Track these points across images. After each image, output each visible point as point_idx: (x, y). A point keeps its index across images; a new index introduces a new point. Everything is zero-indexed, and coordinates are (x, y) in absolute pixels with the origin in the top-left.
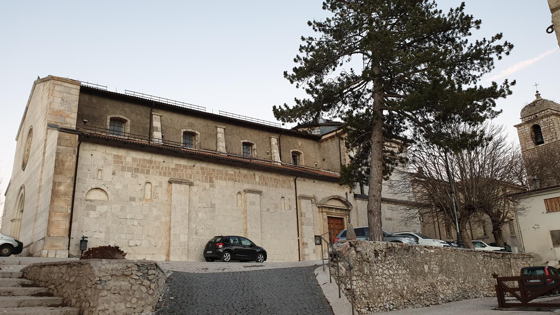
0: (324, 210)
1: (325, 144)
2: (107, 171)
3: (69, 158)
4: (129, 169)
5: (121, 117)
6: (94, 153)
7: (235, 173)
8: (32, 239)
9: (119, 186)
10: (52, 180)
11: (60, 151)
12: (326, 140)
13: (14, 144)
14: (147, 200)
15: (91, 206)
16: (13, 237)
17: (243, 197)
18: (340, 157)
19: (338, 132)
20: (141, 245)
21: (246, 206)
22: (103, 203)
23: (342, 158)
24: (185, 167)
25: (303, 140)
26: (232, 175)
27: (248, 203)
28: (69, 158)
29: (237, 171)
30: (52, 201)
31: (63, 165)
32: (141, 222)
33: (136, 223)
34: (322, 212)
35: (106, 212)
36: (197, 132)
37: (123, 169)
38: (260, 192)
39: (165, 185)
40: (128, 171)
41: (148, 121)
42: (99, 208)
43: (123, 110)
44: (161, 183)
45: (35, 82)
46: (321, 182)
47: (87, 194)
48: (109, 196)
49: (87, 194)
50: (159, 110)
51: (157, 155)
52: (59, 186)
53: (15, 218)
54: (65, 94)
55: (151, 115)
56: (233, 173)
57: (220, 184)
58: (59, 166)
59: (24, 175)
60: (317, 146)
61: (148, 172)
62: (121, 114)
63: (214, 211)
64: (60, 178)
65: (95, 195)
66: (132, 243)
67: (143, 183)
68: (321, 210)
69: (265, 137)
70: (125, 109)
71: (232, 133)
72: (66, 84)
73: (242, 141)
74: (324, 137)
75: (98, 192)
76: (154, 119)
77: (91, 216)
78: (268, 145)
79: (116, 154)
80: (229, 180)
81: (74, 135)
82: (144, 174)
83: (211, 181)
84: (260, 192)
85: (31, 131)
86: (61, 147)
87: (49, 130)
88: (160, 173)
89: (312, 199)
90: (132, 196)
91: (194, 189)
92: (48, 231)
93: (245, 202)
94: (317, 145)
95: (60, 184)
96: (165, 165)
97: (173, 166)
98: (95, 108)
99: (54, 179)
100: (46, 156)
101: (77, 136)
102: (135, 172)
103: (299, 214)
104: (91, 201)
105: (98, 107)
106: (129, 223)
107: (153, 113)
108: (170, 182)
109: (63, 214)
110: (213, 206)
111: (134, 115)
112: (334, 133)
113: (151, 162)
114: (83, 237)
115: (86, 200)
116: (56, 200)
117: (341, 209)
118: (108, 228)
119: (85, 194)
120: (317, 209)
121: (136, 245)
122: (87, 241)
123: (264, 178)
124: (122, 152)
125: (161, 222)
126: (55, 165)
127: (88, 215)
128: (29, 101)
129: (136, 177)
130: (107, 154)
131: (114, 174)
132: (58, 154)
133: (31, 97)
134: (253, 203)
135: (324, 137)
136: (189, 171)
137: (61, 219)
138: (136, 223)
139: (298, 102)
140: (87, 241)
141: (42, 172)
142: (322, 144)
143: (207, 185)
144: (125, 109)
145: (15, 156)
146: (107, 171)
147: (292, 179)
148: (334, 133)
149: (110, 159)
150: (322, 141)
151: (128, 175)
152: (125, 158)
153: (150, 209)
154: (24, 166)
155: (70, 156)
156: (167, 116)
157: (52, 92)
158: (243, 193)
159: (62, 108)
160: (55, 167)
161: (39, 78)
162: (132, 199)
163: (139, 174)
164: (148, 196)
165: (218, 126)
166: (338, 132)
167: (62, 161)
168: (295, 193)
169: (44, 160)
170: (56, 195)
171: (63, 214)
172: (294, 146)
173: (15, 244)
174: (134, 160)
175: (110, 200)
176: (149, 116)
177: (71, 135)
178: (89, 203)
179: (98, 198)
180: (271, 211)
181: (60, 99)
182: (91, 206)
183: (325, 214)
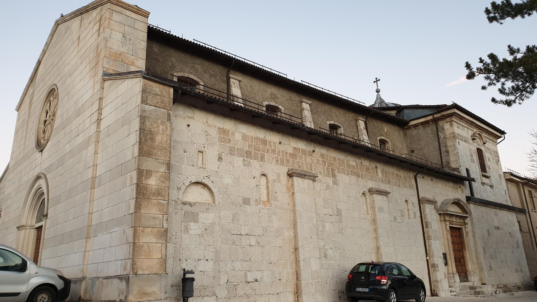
0: (447, 218)
1: (414, 132)
2: (212, 154)
3: (161, 127)
4: (240, 153)
5: (191, 76)
6: (191, 122)
7: (357, 163)
8: (82, 271)
9: (228, 180)
10: (133, 165)
11: (147, 114)
12: (416, 126)
13: (12, 118)
14: (264, 203)
15: (191, 213)
16: (54, 270)
17: (368, 201)
18: (440, 148)
19: (436, 116)
20: (262, 278)
21: (374, 214)
22: (207, 208)
23: (443, 149)
24: (304, 152)
25: (389, 125)
26: (353, 166)
27: (377, 210)
28: (161, 127)
29: (359, 161)
30: (138, 207)
31: (152, 139)
32: (259, 240)
33: (253, 241)
34: (445, 220)
35: (213, 224)
36: (280, 107)
37: (232, 151)
38: (385, 193)
39: (284, 178)
40: (238, 156)
41: (225, 86)
42: (202, 216)
43: (193, 66)
44: (279, 175)
45: (57, 22)
46: (438, 181)
47: (184, 193)
48: (216, 195)
49: (184, 193)
50: (237, 73)
51: (272, 133)
52: (148, 178)
53: (24, 223)
54: (127, 28)
55: (228, 78)
56: (354, 164)
57: (344, 178)
58: (146, 140)
59: (41, 162)
60: (402, 134)
61: (262, 158)
62: (191, 73)
63: (341, 221)
64: (149, 164)
65: (197, 195)
66: (250, 278)
67: (257, 174)
68: (442, 219)
69: (350, 118)
70: (196, 66)
71: (317, 111)
72: (128, 13)
73: (328, 123)
74: (412, 123)
75: (199, 188)
76: (232, 84)
77: (192, 232)
78: (355, 130)
79: (221, 126)
80: (352, 174)
81: (166, 88)
82: (258, 160)
83: (334, 176)
84: (385, 193)
85: (52, 92)
86: (147, 107)
87: (107, 83)
88: (277, 161)
89: (432, 202)
90: (247, 196)
91: (317, 185)
92: (134, 264)
93: (373, 208)
94: (401, 132)
95: (149, 173)
96: (281, 148)
97: (290, 151)
98: (158, 61)
99: (138, 165)
100: (104, 124)
101: (172, 90)
102: (247, 157)
103: (424, 224)
104: (191, 204)
105: (161, 60)
106: (245, 241)
107: (231, 76)
108: (290, 175)
109: (155, 230)
110: (339, 213)
111: (207, 76)
112: (430, 118)
113: (264, 142)
114: (185, 272)
115: (184, 204)
116: (144, 203)
117: (457, 216)
118: (217, 252)
119: (181, 192)
120: (438, 216)
121: (256, 281)
122: (193, 279)
123: (386, 172)
124: (228, 125)
125: (283, 239)
126: (140, 139)
127: (187, 230)
128: (44, 52)
129: (249, 165)
130: (209, 126)
131: (220, 159)
132: (143, 119)
133: (47, 45)
134: (381, 210)
135: (412, 123)
136: (309, 159)
137: (154, 240)
138: (253, 241)
139: (512, 51)
140: (193, 279)
141: (96, 153)
142: (409, 132)
143: (330, 181)
144: (196, 66)
145: (16, 132)
146: (212, 154)
147: (412, 175)
148: (430, 118)
149: (214, 133)
150: (410, 128)
151: (239, 161)
152: (233, 134)
153: (269, 217)
154: (40, 147)
155: (162, 123)
156: (247, 81)
157: (109, 23)
158: (368, 194)
159: (124, 50)
160: (140, 142)
161: (62, 16)
162: (246, 201)
163: (252, 161)
164: (264, 198)
165: (304, 100)
166: (436, 116)
167: (151, 132)
168: (416, 195)
169: (98, 132)
170: (144, 195)
171: (155, 230)
172: (380, 132)
173: (59, 285)
174: (245, 137)
175: (217, 202)
176: (225, 79)
177: (161, 86)
178: (187, 208)
179: (198, 200)
180: (399, 220)
181: (120, 36)
182: (191, 213)
183: (448, 223)
